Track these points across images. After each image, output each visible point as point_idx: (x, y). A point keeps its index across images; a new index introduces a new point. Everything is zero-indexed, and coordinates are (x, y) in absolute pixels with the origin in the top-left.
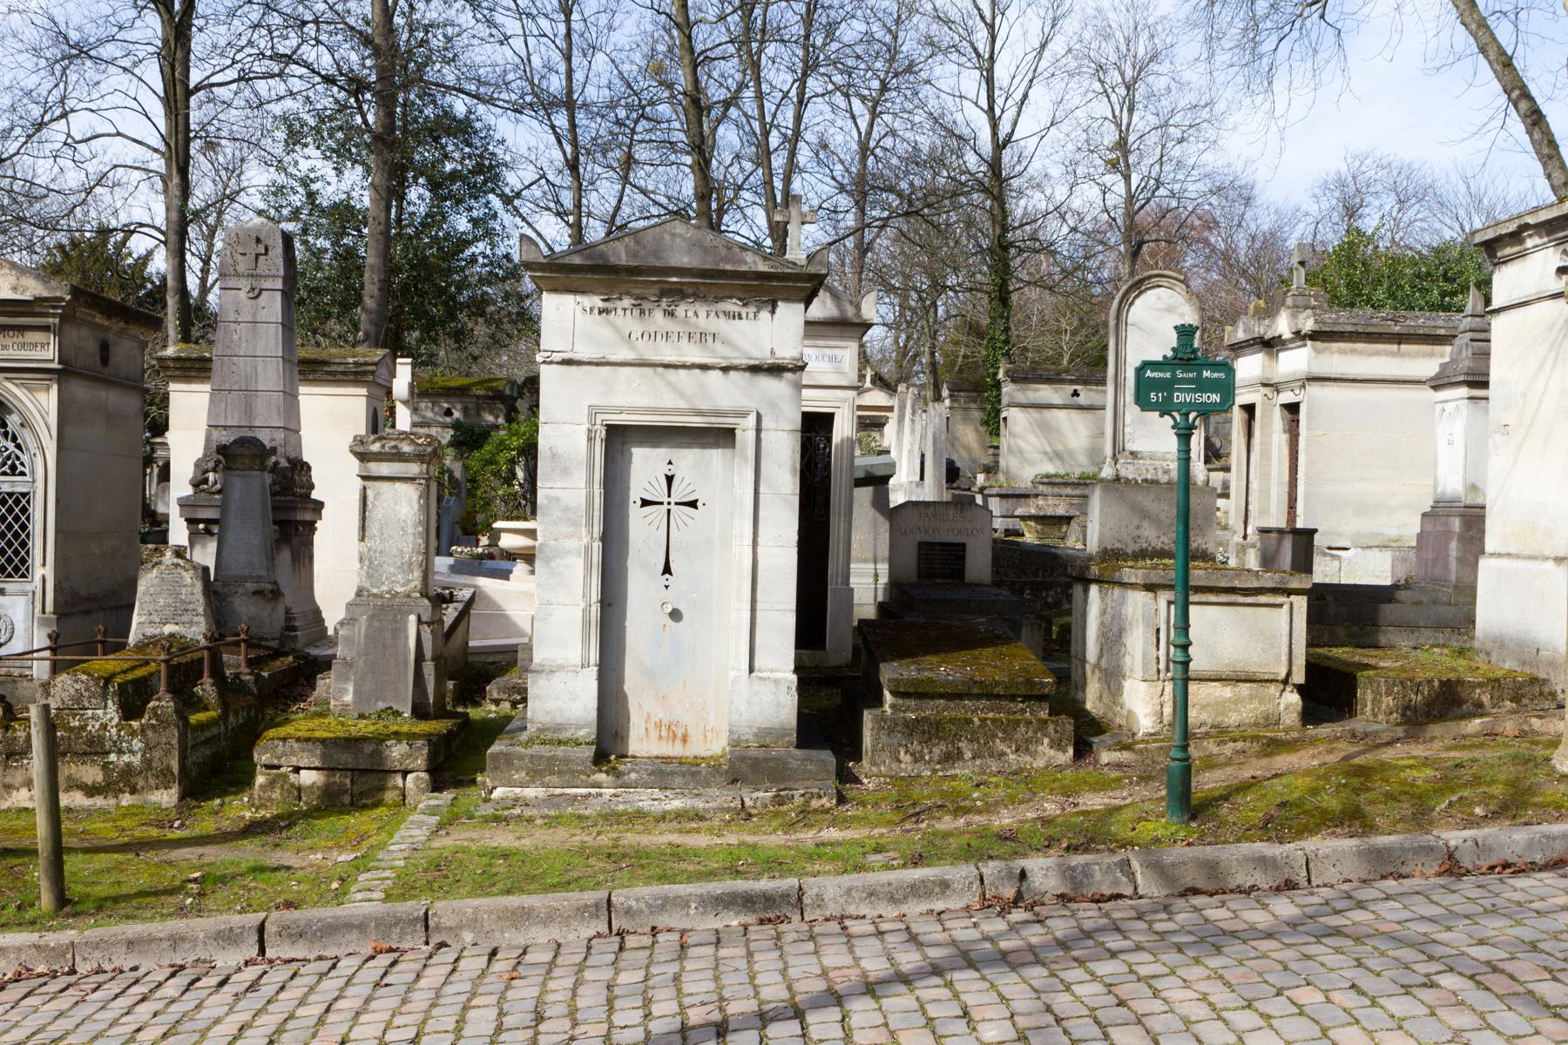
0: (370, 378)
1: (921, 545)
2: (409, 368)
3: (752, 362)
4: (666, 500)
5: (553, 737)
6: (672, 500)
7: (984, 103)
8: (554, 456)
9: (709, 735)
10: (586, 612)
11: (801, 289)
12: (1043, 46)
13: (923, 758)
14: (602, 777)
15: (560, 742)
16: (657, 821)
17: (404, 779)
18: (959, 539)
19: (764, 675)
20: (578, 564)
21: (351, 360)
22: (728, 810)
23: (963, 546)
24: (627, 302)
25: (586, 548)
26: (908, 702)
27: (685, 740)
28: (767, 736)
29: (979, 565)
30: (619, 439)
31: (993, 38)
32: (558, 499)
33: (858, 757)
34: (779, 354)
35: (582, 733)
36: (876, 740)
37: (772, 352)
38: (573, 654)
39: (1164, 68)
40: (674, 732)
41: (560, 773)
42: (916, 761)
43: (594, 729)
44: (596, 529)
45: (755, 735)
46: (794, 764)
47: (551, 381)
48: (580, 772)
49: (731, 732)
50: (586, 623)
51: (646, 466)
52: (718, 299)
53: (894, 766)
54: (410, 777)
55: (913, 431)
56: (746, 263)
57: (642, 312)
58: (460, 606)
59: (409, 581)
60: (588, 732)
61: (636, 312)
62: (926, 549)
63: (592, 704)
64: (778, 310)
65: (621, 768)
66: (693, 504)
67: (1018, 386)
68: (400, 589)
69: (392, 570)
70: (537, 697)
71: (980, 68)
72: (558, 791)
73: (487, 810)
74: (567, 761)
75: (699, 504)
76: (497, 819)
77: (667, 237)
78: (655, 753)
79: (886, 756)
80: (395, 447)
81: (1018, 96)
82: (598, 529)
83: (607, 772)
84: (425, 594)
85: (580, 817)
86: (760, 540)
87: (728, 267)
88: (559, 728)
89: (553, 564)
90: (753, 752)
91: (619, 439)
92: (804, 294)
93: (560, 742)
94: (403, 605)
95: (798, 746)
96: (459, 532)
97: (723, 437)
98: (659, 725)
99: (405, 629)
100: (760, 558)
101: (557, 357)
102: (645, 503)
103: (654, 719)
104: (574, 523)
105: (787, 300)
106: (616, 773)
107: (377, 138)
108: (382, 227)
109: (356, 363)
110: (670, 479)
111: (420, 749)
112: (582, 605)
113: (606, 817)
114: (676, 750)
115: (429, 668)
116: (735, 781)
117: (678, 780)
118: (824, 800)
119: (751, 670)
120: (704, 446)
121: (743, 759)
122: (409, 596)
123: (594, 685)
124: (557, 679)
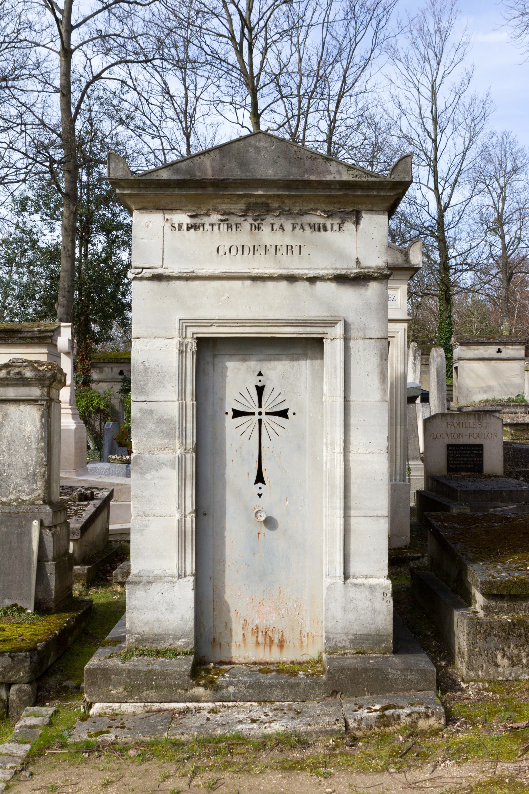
0: (49, 341)
1: (449, 446)
2: (69, 330)
3: (338, 272)
4: (257, 410)
5: (152, 647)
6: (263, 410)
7: (432, 185)
8: (146, 370)
9: (305, 640)
10: (181, 523)
11: (384, 198)
12: (464, 153)
13: (520, 661)
14: (200, 691)
15: (158, 653)
16: (257, 749)
17: (8, 690)
18: (477, 442)
19: (359, 581)
20: (172, 475)
21: (36, 329)
22: (332, 733)
23: (481, 446)
24: (215, 218)
25: (180, 460)
26: (500, 604)
27: (281, 646)
28: (363, 643)
29: (494, 460)
30: (209, 350)
31: (436, 149)
32: (151, 412)
33: (450, 658)
34: (365, 263)
35: (180, 643)
36: (472, 644)
37: (358, 262)
38: (169, 564)
39: (522, 176)
40: (268, 638)
41: (158, 687)
42: (513, 665)
43: (192, 639)
44: (189, 441)
45: (352, 641)
46: (394, 674)
47: (141, 297)
48: (178, 687)
49: (328, 639)
50: (181, 534)
51: (238, 378)
52: (302, 213)
53: (492, 670)
54: (14, 689)
55: (415, 371)
56: (330, 173)
57: (229, 227)
58: (98, 503)
59: (33, 490)
60: (184, 643)
61: (224, 227)
62: (453, 450)
63: (190, 614)
64: (362, 222)
65: (220, 680)
66: (283, 414)
67: (463, 348)
68: (25, 498)
69: (18, 481)
70: (135, 608)
71: (429, 165)
72: (156, 706)
73: (81, 734)
74: (164, 675)
75: (289, 414)
76: (89, 748)
77: (251, 150)
78: (253, 659)
79: (483, 660)
80: (19, 373)
81: (452, 180)
82: (191, 441)
83: (205, 686)
84: (48, 501)
85: (177, 745)
86: (352, 448)
87: (313, 178)
88: (158, 638)
89: (148, 476)
90: (351, 661)
91: (209, 350)
92: (387, 205)
93: (158, 653)
94: (27, 511)
95: (395, 651)
96: (116, 445)
97: (314, 346)
98: (256, 631)
99: (29, 534)
100: (353, 466)
101: (147, 273)
102: (237, 414)
103: (251, 626)
104: (168, 435)
105: (371, 210)
106: (211, 684)
107: (66, 195)
108: (70, 253)
109: (39, 331)
110: (260, 390)
111: (22, 661)
112: (177, 516)
113: (202, 743)
114: (273, 655)
115: (50, 567)
116: (334, 693)
117: (277, 693)
118: (432, 721)
119: (346, 577)
120: (293, 358)
121: (342, 670)
122: (33, 503)
123: (191, 595)
124: (155, 589)
